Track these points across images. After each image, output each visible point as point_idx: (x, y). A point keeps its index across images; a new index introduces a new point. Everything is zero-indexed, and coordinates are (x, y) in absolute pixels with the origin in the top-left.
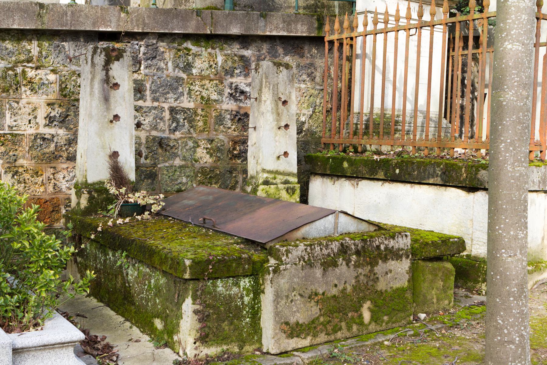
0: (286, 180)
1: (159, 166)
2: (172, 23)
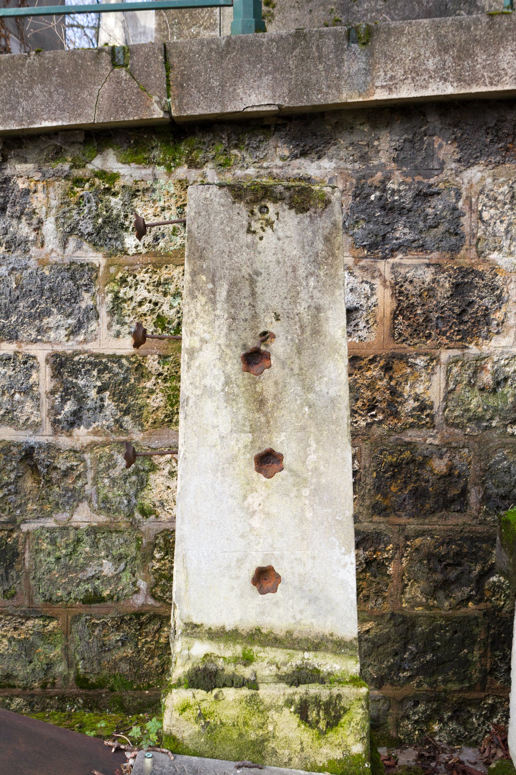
0: (300, 669)
1: (25, 528)
2: (27, 98)
